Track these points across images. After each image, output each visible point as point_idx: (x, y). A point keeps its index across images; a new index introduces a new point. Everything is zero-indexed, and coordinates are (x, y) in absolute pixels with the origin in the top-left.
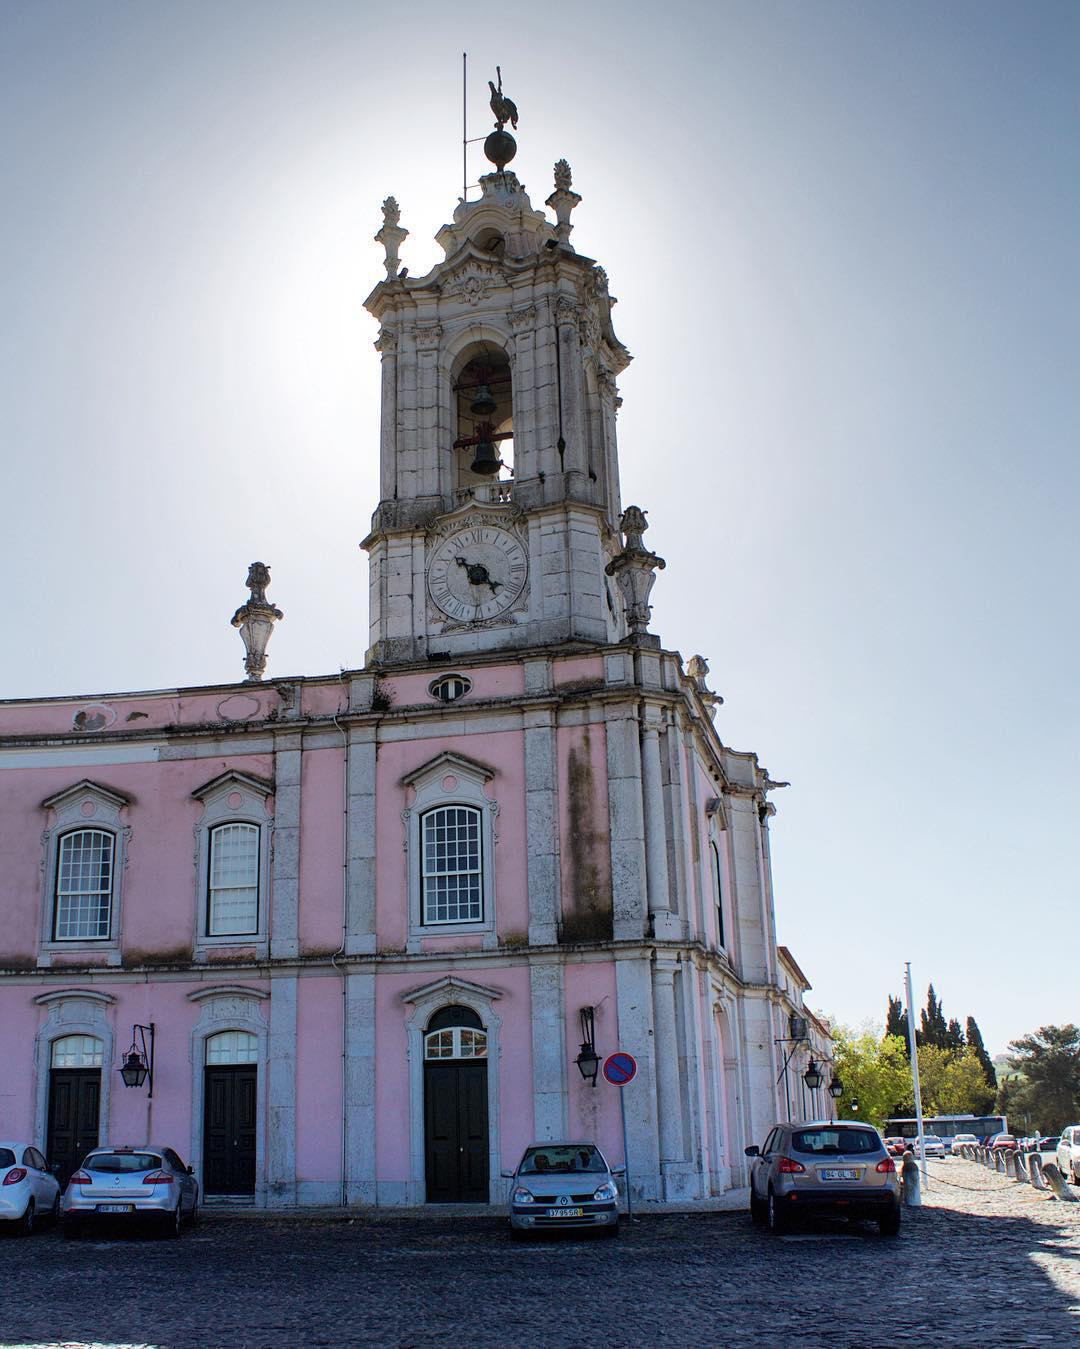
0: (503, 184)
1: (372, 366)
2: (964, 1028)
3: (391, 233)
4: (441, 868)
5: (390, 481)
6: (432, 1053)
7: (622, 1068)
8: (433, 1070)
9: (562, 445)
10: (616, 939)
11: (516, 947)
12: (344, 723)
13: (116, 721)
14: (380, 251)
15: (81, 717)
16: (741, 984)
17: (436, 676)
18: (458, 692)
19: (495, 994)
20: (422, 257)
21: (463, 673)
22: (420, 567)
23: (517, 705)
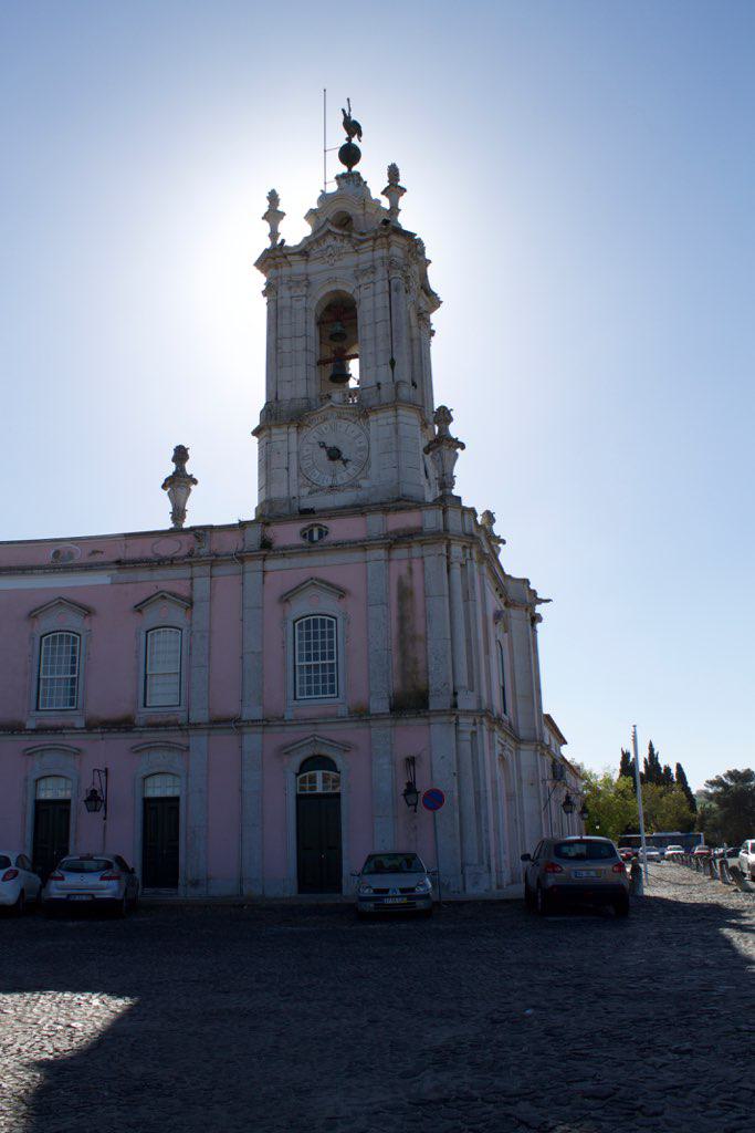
1: (261, 305)
3: (274, 215)
4: (308, 659)
6: (302, 789)
7: (435, 799)
8: (305, 802)
9: (393, 363)
11: (361, 714)
12: (241, 557)
13: (81, 556)
14: (266, 227)
15: (57, 554)
16: (518, 740)
19: (346, 748)
20: (295, 231)
21: (324, 523)
22: (294, 448)
23: (362, 545)
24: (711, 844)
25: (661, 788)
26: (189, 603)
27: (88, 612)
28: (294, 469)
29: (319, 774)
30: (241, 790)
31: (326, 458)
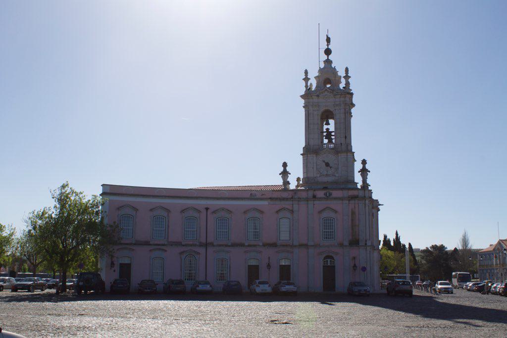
0: (328, 62)
1: (302, 112)
2: (407, 246)
3: (306, 79)
5: (308, 141)
6: (324, 264)
8: (325, 267)
10: (360, 244)
11: (341, 245)
12: (307, 199)
13: (259, 196)
14: (304, 83)
15: (251, 194)
17: (325, 192)
18: (329, 195)
20: (313, 83)
23: (342, 199)
24: (423, 281)
25: (401, 254)
26: (292, 212)
27: (262, 212)
28: (315, 169)
29: (329, 260)
30: (308, 264)
31: (325, 166)
